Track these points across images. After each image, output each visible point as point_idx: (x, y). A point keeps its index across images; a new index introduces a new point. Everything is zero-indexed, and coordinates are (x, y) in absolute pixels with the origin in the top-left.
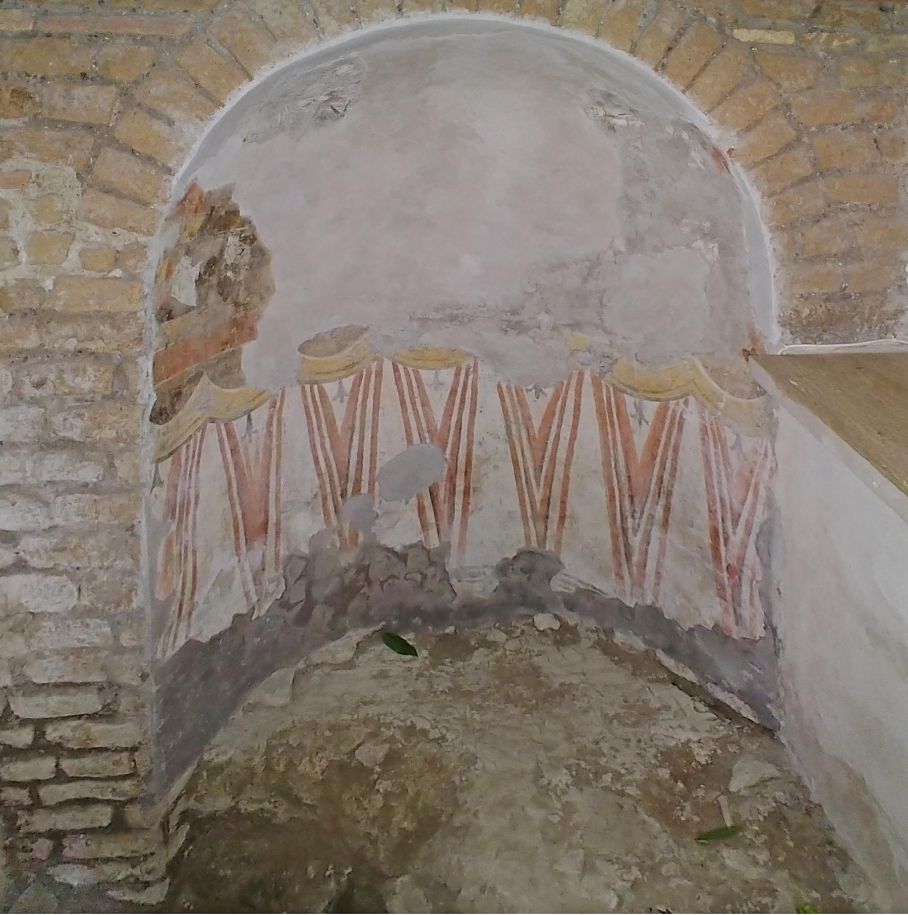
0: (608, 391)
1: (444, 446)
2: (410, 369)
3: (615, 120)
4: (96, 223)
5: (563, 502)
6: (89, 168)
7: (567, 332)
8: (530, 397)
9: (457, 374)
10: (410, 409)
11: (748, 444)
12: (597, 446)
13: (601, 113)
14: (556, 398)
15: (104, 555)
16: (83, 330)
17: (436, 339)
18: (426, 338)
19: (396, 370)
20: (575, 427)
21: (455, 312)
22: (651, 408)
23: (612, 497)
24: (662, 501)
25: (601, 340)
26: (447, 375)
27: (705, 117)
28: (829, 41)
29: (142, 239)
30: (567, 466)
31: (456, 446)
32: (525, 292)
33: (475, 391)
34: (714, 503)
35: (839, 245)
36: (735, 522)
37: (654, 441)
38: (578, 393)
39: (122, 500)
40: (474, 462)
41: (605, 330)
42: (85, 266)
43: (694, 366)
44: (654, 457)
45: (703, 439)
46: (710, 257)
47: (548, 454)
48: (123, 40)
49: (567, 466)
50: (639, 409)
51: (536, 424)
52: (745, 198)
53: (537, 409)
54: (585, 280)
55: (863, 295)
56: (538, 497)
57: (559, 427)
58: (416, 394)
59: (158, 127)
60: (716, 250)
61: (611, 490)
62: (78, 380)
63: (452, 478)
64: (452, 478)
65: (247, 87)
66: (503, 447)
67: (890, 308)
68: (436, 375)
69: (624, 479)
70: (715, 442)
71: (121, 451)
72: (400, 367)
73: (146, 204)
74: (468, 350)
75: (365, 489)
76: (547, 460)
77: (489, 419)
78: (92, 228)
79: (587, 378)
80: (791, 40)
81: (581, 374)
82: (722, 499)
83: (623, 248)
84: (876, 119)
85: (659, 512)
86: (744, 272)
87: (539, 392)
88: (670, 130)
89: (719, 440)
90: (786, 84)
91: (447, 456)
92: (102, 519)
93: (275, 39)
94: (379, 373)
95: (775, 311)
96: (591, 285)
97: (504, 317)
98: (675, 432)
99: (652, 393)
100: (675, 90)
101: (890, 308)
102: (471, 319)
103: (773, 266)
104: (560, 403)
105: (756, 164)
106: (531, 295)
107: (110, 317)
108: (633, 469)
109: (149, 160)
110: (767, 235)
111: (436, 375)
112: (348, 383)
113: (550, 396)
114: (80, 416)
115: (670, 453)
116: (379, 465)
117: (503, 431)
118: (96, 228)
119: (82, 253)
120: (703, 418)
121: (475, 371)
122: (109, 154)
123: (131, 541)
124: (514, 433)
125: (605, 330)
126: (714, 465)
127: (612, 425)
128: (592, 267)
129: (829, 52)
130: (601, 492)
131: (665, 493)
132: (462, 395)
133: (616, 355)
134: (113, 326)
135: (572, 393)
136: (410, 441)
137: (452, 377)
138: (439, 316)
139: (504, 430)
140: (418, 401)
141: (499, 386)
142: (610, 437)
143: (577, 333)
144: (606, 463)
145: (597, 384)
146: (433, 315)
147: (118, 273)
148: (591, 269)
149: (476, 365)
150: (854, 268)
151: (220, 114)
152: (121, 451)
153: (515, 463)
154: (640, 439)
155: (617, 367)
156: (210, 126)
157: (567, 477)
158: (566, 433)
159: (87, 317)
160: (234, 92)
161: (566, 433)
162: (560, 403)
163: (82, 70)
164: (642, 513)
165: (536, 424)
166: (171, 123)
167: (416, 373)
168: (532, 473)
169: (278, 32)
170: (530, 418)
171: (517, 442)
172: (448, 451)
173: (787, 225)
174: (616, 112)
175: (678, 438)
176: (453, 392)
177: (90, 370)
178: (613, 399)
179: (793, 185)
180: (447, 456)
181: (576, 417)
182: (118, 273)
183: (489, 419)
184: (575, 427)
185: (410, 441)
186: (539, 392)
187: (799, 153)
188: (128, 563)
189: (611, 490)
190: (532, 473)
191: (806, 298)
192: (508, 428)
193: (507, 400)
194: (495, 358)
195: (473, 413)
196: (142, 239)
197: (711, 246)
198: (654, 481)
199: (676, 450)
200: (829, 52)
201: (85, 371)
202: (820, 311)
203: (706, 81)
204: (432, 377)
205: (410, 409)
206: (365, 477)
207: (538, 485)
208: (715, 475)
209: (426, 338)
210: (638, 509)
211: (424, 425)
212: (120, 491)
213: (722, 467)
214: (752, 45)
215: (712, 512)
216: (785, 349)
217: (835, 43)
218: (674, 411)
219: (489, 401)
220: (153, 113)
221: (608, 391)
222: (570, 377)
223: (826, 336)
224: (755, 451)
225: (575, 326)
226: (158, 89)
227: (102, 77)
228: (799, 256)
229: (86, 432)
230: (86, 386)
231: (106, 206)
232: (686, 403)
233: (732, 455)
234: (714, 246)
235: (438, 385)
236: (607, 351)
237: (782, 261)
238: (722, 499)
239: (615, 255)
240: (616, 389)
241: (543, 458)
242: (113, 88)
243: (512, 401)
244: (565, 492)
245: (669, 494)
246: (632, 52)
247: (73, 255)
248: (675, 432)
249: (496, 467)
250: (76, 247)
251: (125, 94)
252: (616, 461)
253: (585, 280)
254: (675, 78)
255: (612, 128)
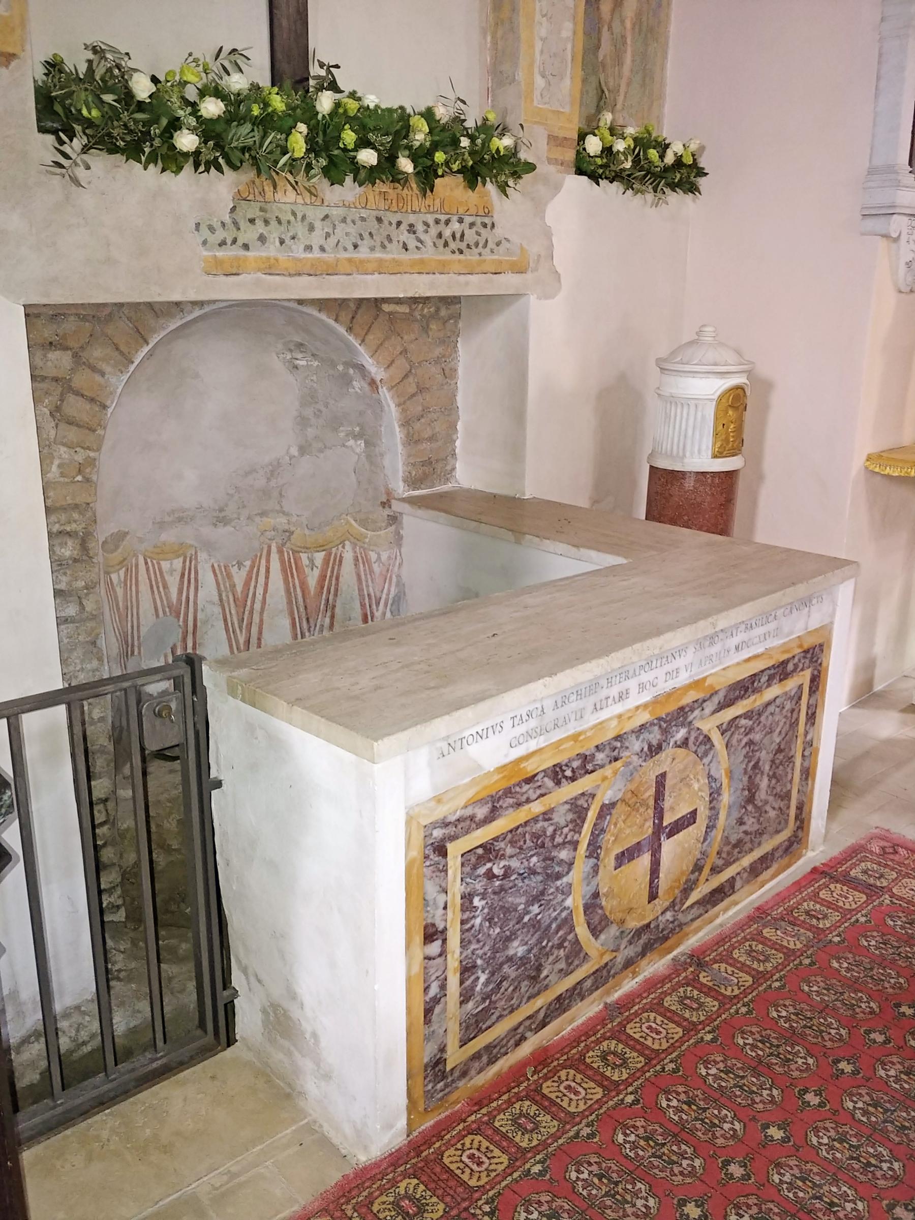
0: (288, 554)
1: (178, 617)
2: (155, 562)
3: (298, 362)
4: (64, 445)
5: (259, 639)
6: (58, 409)
7: (258, 519)
8: (234, 570)
9: (184, 562)
10: (156, 592)
11: (384, 556)
12: (282, 592)
13: (289, 357)
14: (252, 567)
15: (82, 662)
16: (63, 517)
17: (169, 536)
18: (164, 537)
19: (146, 563)
20: (266, 584)
21: (181, 514)
22: (319, 557)
23: (294, 624)
24: (329, 614)
25: (282, 520)
26: (178, 563)
27: (370, 360)
28: (422, 309)
29: (92, 454)
30: (262, 613)
31: (186, 615)
32: (228, 494)
33: (196, 573)
34: (364, 599)
35: (427, 433)
36: (378, 604)
37: (323, 577)
38: (268, 561)
39: (90, 624)
40: (199, 624)
41: (284, 513)
42: (62, 475)
43: (348, 522)
44: (322, 588)
45: (356, 565)
46: (358, 450)
47: (248, 608)
48: (72, 318)
49: (262, 613)
50: (311, 561)
51: (239, 588)
52: (386, 408)
53: (239, 577)
54: (269, 479)
55: (437, 461)
56: (242, 640)
57: (255, 587)
58: (159, 580)
59: (98, 378)
60: (363, 445)
61: (293, 619)
62: (63, 550)
63: (184, 639)
64: (184, 639)
65: (146, 349)
66: (217, 610)
67: (449, 468)
68: (171, 564)
69: (302, 609)
70: (364, 563)
71: (87, 595)
72: (149, 560)
73: (94, 431)
74: (192, 542)
75: (136, 653)
76: (247, 613)
77: (208, 589)
78: (63, 449)
79: (274, 549)
80: (407, 311)
81: (269, 547)
82: (369, 595)
83: (296, 454)
84: (444, 356)
85: (327, 620)
86: (382, 455)
87: (240, 565)
88: (340, 368)
89: (367, 561)
90: (406, 337)
91: (181, 624)
92: (81, 638)
93: (157, 316)
94: (137, 566)
95: (401, 474)
96: (273, 483)
97: (215, 515)
98: (336, 567)
99: (320, 548)
100: (356, 343)
101: (449, 468)
102: (192, 518)
103: (400, 448)
104: (255, 569)
105: (392, 387)
106: (232, 496)
107: (76, 507)
108: (308, 601)
109: (92, 400)
110: (397, 429)
111: (171, 564)
112: (122, 572)
113: (247, 569)
114: (65, 574)
115: (334, 582)
116: (142, 634)
117: (216, 599)
118: (65, 449)
119: (59, 466)
120: (355, 552)
121: (196, 558)
122: (71, 398)
123: (95, 650)
124: (224, 598)
125: (284, 513)
126: (363, 577)
127: (292, 577)
128: (274, 470)
129: (423, 316)
130: (287, 622)
131: (330, 607)
132: (189, 577)
133: (292, 529)
134: (80, 513)
135: (263, 562)
136: (157, 616)
137: (181, 564)
138: (170, 519)
139: (217, 598)
140: (160, 585)
141: (213, 566)
142: (291, 585)
143: (265, 519)
144: (290, 602)
145: (280, 552)
146: (167, 519)
147: (79, 478)
148: (272, 472)
149: (196, 553)
150: (434, 445)
151: (132, 368)
152: (87, 595)
153: (225, 620)
154: (312, 581)
155: (293, 537)
156: (125, 377)
157: (261, 621)
158: (260, 590)
159: (64, 509)
160: (139, 353)
161: (260, 590)
162: (255, 569)
163: (50, 340)
164: (316, 625)
165: (239, 588)
166: (103, 374)
167: (159, 564)
168: (236, 625)
169: (159, 312)
170: (234, 586)
171: (226, 605)
172: (181, 619)
173: (406, 423)
174: (300, 356)
175: (339, 570)
176: (183, 575)
177: (70, 543)
178: (292, 560)
179: (409, 399)
180: (181, 624)
181: (267, 578)
182: (79, 478)
183: (208, 589)
184: (266, 584)
185: (157, 616)
186: (240, 565)
187: (411, 379)
188: (95, 663)
189: (293, 619)
190: (236, 625)
191: (413, 465)
192: (220, 595)
193: (219, 575)
194: (209, 546)
195: (196, 589)
196: (92, 454)
197: (359, 442)
198: (323, 602)
199: (337, 579)
200: (423, 316)
201: (66, 544)
202: (420, 472)
203: (370, 337)
204: (169, 566)
205: (156, 592)
206: (136, 643)
207: (241, 631)
208: (364, 583)
209: (164, 537)
210: (312, 625)
211: (165, 602)
212: (88, 619)
213: (369, 576)
214: (390, 313)
215: (363, 605)
216: (406, 494)
217: (426, 310)
218: (336, 554)
219: (207, 579)
220: (93, 369)
221: (288, 554)
222: (262, 549)
223: (422, 486)
224: (389, 558)
225: (263, 514)
226: (97, 353)
227: (61, 344)
228: (412, 440)
229: (69, 583)
230: (68, 554)
231: (72, 434)
232: (343, 547)
233: (376, 567)
234: (362, 443)
235: (172, 571)
236: (286, 527)
237: (403, 444)
238: (369, 595)
239: (290, 459)
240: (294, 552)
241: (244, 613)
242: (69, 352)
243: (223, 575)
244: (260, 632)
245: (334, 607)
246: (336, 320)
247: (54, 468)
248: (336, 567)
249: (212, 626)
250: (56, 462)
251: (76, 356)
252: (296, 599)
253: (269, 479)
254: (356, 336)
255: (296, 367)
